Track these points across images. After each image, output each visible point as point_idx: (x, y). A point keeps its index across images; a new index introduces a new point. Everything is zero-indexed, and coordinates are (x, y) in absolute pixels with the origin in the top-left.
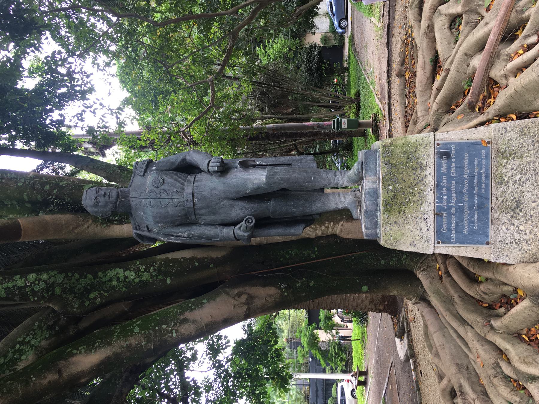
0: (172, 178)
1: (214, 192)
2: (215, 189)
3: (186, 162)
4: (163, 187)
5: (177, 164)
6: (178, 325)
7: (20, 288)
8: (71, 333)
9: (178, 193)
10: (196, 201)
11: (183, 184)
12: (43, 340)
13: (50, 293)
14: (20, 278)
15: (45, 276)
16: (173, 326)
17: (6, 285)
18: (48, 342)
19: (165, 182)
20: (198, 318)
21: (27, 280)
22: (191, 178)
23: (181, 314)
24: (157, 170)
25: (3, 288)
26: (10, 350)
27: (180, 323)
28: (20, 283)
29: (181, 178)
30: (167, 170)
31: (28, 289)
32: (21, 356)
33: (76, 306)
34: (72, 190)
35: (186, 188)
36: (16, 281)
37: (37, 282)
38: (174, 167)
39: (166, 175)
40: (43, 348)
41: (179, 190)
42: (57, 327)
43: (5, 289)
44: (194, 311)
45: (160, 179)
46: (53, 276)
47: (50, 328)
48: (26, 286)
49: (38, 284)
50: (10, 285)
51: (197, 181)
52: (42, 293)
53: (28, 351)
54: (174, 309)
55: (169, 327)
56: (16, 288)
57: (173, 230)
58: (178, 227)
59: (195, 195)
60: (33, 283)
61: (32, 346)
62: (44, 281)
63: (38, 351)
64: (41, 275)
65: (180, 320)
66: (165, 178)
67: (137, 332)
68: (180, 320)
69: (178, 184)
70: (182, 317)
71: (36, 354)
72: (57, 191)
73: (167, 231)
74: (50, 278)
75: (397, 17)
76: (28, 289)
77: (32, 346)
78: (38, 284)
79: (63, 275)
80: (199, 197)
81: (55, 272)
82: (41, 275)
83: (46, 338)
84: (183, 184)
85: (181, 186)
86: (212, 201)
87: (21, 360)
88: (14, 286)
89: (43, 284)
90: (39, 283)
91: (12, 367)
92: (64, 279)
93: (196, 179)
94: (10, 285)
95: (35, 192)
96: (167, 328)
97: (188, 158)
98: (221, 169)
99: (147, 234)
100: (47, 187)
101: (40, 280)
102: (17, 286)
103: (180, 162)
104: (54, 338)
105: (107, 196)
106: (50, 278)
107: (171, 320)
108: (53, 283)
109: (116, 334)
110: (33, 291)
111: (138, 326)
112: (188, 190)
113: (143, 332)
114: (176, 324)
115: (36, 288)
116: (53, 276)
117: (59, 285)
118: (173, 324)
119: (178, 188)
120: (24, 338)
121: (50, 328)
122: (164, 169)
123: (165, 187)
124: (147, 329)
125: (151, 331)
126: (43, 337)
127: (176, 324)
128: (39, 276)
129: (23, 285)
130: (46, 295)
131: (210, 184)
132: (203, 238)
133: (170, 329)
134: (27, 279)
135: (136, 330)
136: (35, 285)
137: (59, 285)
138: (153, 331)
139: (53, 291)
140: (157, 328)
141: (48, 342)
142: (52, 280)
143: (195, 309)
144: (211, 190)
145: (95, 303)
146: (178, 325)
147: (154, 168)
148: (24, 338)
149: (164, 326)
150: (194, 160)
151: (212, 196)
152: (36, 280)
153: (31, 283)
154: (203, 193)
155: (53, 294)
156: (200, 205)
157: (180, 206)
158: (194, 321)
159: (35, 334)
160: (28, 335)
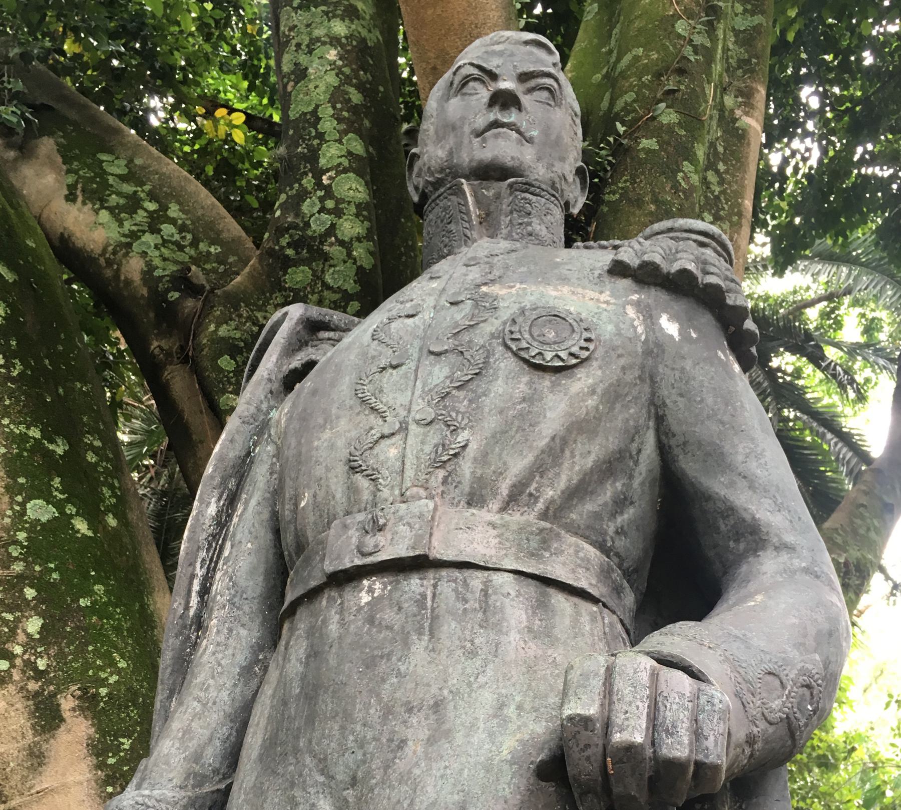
0: (580, 427)
1: (417, 730)
2: (439, 734)
3: (741, 558)
4: (506, 364)
5: (718, 486)
6: (33, 686)
7: (313, 156)
8: (155, 344)
9: (445, 460)
10: (366, 593)
11: (517, 497)
12: (149, 264)
13: (290, 252)
14: (350, 153)
15: (350, 227)
16: (30, 665)
17: (326, 111)
18: (137, 278)
19: (546, 381)
20: (46, 780)
21: (338, 173)
22: (574, 560)
23: (88, 703)
24: (655, 348)
25: (317, 106)
26: (147, 188)
27: (37, 694)
28: (331, 154)
29: (577, 492)
30: (660, 420)
31: (308, 182)
32: (111, 210)
33: (223, 331)
34: (655, 201)
35: (488, 514)
36: (340, 141)
37: (330, 204)
38: (689, 466)
39: (613, 396)
40: (120, 265)
41: (466, 468)
42: (176, 295)
43: (314, 112)
44: (91, 761)
45: (574, 344)
46: (349, 255)
47: (182, 281)
48: (318, 173)
49: (322, 210)
50: (328, 125)
51: (541, 606)
52: (295, 227)
53: (121, 225)
54: (119, 672)
55: (30, 644)
56: (316, 142)
57: (253, 502)
58: (266, 537)
59: (414, 584)
60: (329, 192)
61: (134, 236)
62: (333, 226)
63: (114, 253)
64: (357, 215)
65: (53, 695)
66: (582, 381)
67: (23, 513)
68: (53, 695)
69: (517, 465)
70: (67, 703)
71: (105, 250)
72: (648, 151)
73: (261, 476)
74: (341, 243)
75: (574, 539)
76: (308, 182)
77: (134, 236)
78: (322, 210)
79: (351, 286)
80: (389, 615)
81: (367, 262)
82: (357, 215)
83: (148, 272)
84: (517, 497)
85: (504, 490)
86: (348, 716)
87: (97, 212)
88: (321, 136)
89: (323, 223)
90: (329, 212)
91: (83, 191)
92: (339, 290)
93: (559, 600)
94: (328, 125)
95: (647, 78)
96: (21, 637)
97: (769, 565)
98: (583, 766)
99: (270, 364)
100: (668, 116)
101: (338, 212)
102: (320, 145)
103: (730, 510)
104: (145, 292)
105: (496, 114)
106: (341, 243)
107: (61, 656)
108: (326, 257)
109: (35, 433)
110: (303, 194)
111: (62, 523)
112: (472, 535)
113: (22, 536)
114: (39, 675)
115: (313, 205)
116: (349, 255)
117: (318, 277)
118: (42, 664)
119: (483, 458)
120: (173, 221)
121: (182, 281)
122: (664, 392)
123: (507, 383)
124: (32, 552)
125: (18, 567)
126: (157, 262)
127: (39, 675)
128: (353, 210)
129: (322, 162)
130: (284, 241)
131: (487, 697)
132: (170, 697)
133: (18, 650)
134: (345, 171)
135: (39, 511)
136: (322, 200)
137: (318, 277)
138: (20, 577)
139: (296, 263)
140: (30, 593)
141: (137, 278)
142: (336, 251)
143: (101, 766)
144: (437, 706)
145: (224, 391)
146: (33, 686)
147: (670, 327)
148: (173, 221)
149: (34, 625)
150: (751, 596)
151: (388, 712)
152: (339, 201)
153: (328, 189)
154: (419, 647)
155: (287, 263)
156: (333, 627)
157: (352, 490)
158: (36, 758)
159: (181, 248)
160: (182, 229)
